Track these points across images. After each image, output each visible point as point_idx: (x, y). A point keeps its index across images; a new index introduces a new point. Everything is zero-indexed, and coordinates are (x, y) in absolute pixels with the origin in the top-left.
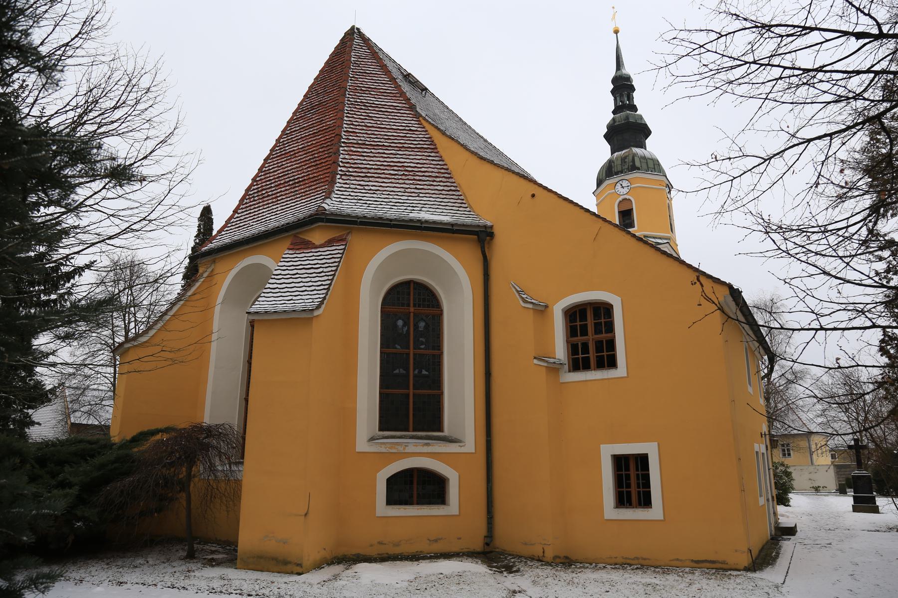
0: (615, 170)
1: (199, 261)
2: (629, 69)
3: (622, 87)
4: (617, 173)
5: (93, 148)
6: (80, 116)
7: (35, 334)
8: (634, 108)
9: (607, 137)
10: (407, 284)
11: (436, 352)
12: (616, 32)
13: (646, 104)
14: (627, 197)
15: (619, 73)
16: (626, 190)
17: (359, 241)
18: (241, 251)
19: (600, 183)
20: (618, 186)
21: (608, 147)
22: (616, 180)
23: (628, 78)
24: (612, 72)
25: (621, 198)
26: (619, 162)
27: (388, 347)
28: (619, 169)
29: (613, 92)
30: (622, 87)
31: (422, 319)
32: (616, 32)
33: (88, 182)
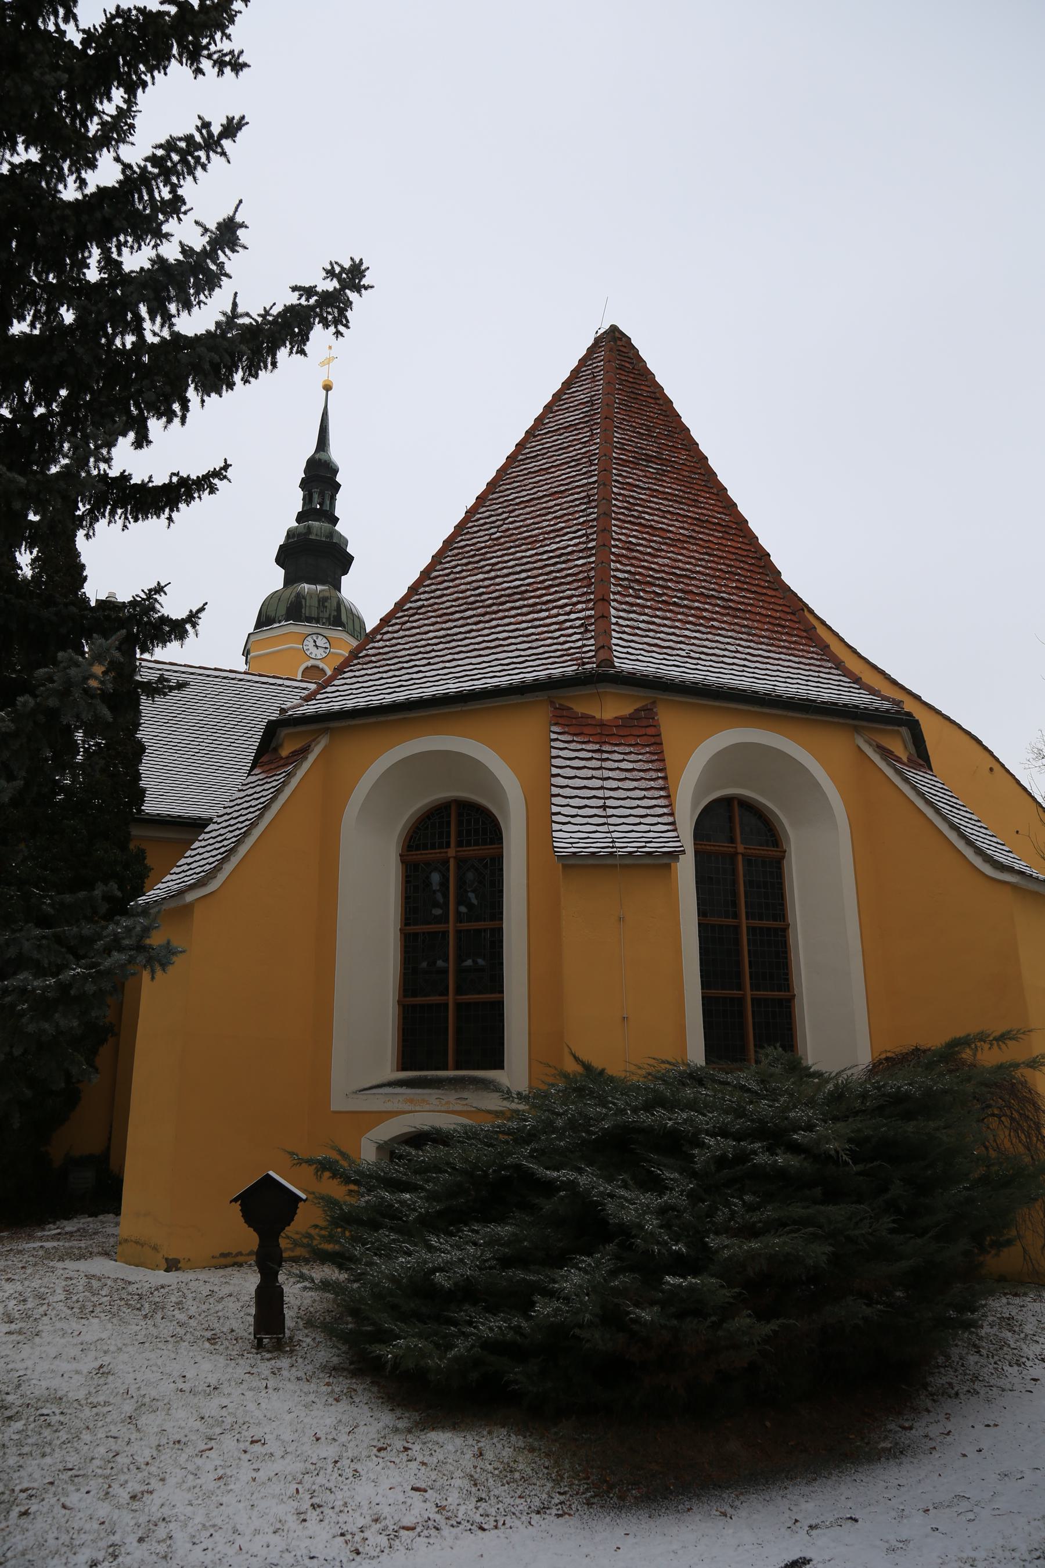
0: (306, 612)
1: (284, 732)
2: (336, 453)
3: (320, 479)
4: (309, 620)
5: (381, 1272)
6: (307, 1261)
8: (335, 520)
9: (284, 557)
12: (327, 388)
14: (321, 665)
15: (317, 456)
16: (320, 653)
17: (673, 723)
19: (264, 620)
20: (309, 643)
23: (332, 470)
24: (309, 448)
26: (315, 603)
28: (314, 614)
29: (304, 484)
32: (327, 388)
33: (192, 887)
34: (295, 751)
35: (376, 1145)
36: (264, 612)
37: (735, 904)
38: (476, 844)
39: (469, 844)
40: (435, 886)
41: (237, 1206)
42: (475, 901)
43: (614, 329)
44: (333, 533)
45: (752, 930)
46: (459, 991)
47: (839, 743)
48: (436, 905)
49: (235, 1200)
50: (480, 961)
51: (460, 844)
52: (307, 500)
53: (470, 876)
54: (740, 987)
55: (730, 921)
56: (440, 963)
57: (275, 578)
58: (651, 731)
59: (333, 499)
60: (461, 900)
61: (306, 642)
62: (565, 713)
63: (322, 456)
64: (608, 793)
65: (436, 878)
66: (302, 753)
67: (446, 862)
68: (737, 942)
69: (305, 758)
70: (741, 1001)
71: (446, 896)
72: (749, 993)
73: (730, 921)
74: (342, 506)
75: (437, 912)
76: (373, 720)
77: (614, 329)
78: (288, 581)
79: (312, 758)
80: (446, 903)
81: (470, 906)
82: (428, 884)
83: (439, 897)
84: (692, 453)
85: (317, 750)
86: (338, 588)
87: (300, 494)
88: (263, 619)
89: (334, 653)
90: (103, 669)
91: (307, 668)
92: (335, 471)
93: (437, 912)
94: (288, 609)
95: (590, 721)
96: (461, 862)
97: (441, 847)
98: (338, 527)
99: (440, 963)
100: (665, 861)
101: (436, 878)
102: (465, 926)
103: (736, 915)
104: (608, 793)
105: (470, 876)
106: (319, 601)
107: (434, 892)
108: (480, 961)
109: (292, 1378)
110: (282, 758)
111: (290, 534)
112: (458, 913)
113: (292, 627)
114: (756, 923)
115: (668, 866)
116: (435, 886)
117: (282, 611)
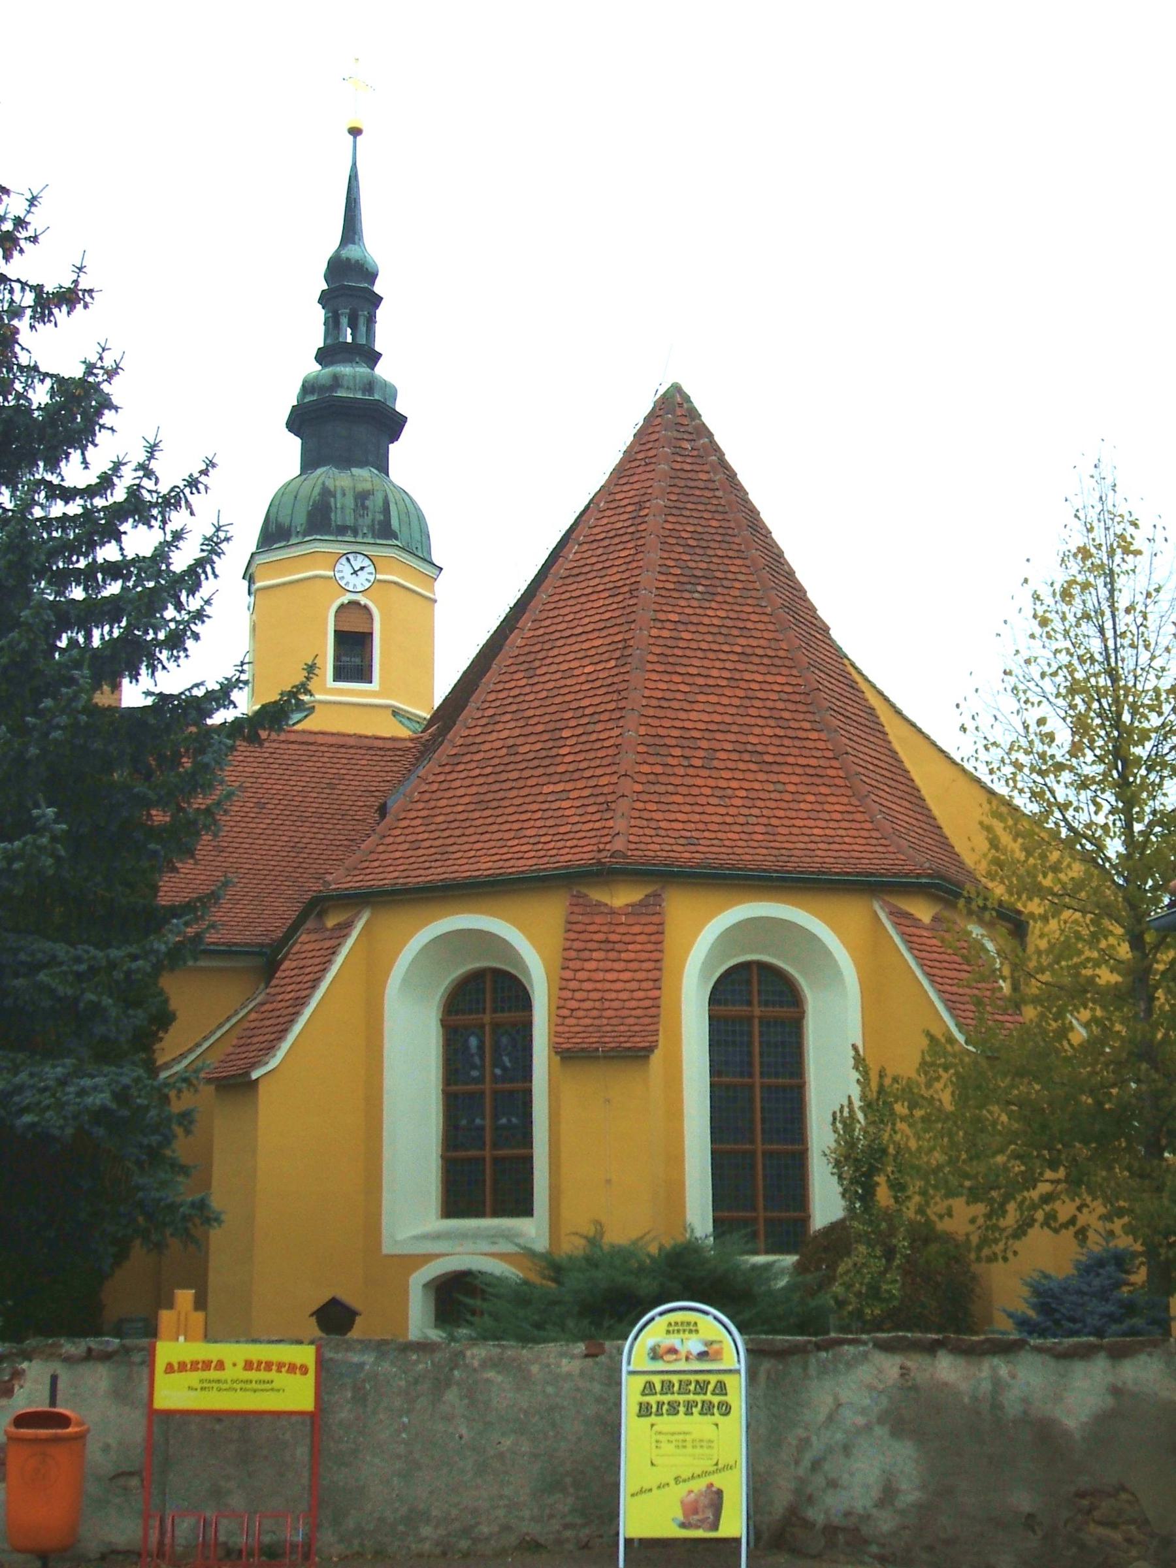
0: (337, 518)
2: (376, 245)
3: (350, 292)
4: (342, 530)
7: (595, 1482)
8: (373, 358)
9: (298, 421)
10: (746, 966)
11: (719, 1214)
12: (355, 132)
13: (406, 356)
14: (363, 600)
16: (361, 582)
18: (950, 883)
21: (293, 445)
22: (342, 549)
24: (330, 241)
25: (346, 598)
26: (350, 502)
27: (455, 1148)
28: (350, 521)
29: (325, 299)
30: (350, 292)
31: (473, 1033)
34: (338, 924)
35: (880, 1431)
36: (272, 516)
37: (751, 1064)
38: (510, 1010)
39: (503, 1011)
40: (474, 1050)
41: (313, 1320)
42: (508, 1064)
43: (676, 389)
44: (371, 385)
45: (766, 1088)
46: (495, 1146)
47: (856, 911)
48: (474, 1067)
49: (312, 1315)
50: (514, 1120)
51: (495, 1011)
52: (332, 325)
53: (504, 1040)
54: (752, 1141)
55: (746, 1080)
56: (478, 1121)
57: (288, 452)
58: (655, 919)
59: (371, 320)
60: (497, 1063)
61: (339, 567)
62: (581, 901)
63: (352, 252)
64: (608, 986)
65: (473, 1042)
66: (348, 926)
67: (483, 1026)
68: (751, 1100)
69: (346, 936)
70: (753, 1153)
71: (482, 1058)
72: (759, 1147)
73: (746, 1080)
74: (388, 332)
75: (475, 1073)
76: (408, 897)
77: (676, 389)
78: (309, 462)
79: (355, 934)
80: (483, 1066)
81: (504, 1069)
82: (466, 1047)
83: (477, 1060)
84: (748, 562)
85: (359, 925)
86: (384, 469)
87: (320, 314)
88: (272, 528)
89: (380, 581)
90: (480, 1527)
91: (342, 606)
92: (372, 276)
93: (475, 1073)
94: (310, 515)
95: (603, 909)
96: (496, 1026)
97: (478, 1012)
98: (382, 370)
99: (478, 1121)
100: (642, 1054)
101: (473, 1042)
102: (500, 1086)
103: (751, 1075)
104: (608, 986)
105: (504, 1040)
106: (356, 499)
107: (472, 1055)
108: (514, 1120)
109: (339, 495)
110: (327, 930)
111: (308, 387)
112: (494, 1075)
113: (317, 544)
114: (772, 1081)
115: (647, 1057)
116: (474, 1050)
117: (301, 519)
